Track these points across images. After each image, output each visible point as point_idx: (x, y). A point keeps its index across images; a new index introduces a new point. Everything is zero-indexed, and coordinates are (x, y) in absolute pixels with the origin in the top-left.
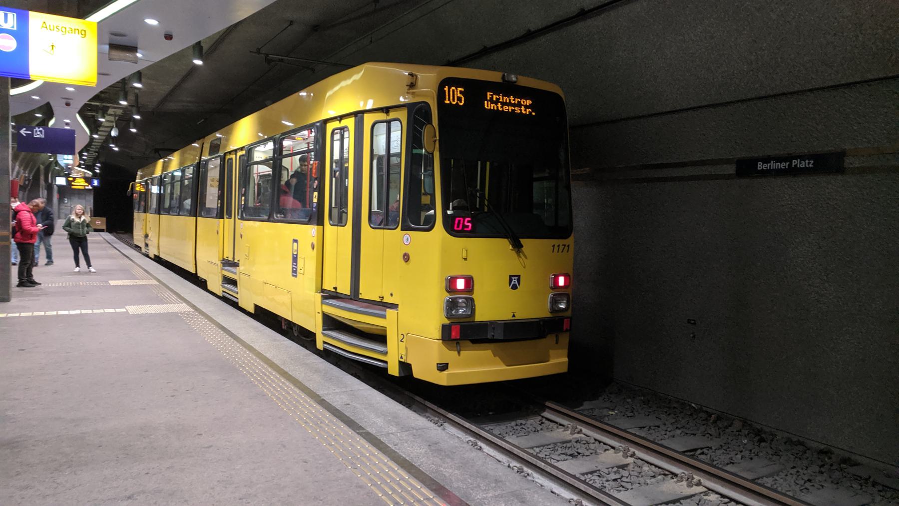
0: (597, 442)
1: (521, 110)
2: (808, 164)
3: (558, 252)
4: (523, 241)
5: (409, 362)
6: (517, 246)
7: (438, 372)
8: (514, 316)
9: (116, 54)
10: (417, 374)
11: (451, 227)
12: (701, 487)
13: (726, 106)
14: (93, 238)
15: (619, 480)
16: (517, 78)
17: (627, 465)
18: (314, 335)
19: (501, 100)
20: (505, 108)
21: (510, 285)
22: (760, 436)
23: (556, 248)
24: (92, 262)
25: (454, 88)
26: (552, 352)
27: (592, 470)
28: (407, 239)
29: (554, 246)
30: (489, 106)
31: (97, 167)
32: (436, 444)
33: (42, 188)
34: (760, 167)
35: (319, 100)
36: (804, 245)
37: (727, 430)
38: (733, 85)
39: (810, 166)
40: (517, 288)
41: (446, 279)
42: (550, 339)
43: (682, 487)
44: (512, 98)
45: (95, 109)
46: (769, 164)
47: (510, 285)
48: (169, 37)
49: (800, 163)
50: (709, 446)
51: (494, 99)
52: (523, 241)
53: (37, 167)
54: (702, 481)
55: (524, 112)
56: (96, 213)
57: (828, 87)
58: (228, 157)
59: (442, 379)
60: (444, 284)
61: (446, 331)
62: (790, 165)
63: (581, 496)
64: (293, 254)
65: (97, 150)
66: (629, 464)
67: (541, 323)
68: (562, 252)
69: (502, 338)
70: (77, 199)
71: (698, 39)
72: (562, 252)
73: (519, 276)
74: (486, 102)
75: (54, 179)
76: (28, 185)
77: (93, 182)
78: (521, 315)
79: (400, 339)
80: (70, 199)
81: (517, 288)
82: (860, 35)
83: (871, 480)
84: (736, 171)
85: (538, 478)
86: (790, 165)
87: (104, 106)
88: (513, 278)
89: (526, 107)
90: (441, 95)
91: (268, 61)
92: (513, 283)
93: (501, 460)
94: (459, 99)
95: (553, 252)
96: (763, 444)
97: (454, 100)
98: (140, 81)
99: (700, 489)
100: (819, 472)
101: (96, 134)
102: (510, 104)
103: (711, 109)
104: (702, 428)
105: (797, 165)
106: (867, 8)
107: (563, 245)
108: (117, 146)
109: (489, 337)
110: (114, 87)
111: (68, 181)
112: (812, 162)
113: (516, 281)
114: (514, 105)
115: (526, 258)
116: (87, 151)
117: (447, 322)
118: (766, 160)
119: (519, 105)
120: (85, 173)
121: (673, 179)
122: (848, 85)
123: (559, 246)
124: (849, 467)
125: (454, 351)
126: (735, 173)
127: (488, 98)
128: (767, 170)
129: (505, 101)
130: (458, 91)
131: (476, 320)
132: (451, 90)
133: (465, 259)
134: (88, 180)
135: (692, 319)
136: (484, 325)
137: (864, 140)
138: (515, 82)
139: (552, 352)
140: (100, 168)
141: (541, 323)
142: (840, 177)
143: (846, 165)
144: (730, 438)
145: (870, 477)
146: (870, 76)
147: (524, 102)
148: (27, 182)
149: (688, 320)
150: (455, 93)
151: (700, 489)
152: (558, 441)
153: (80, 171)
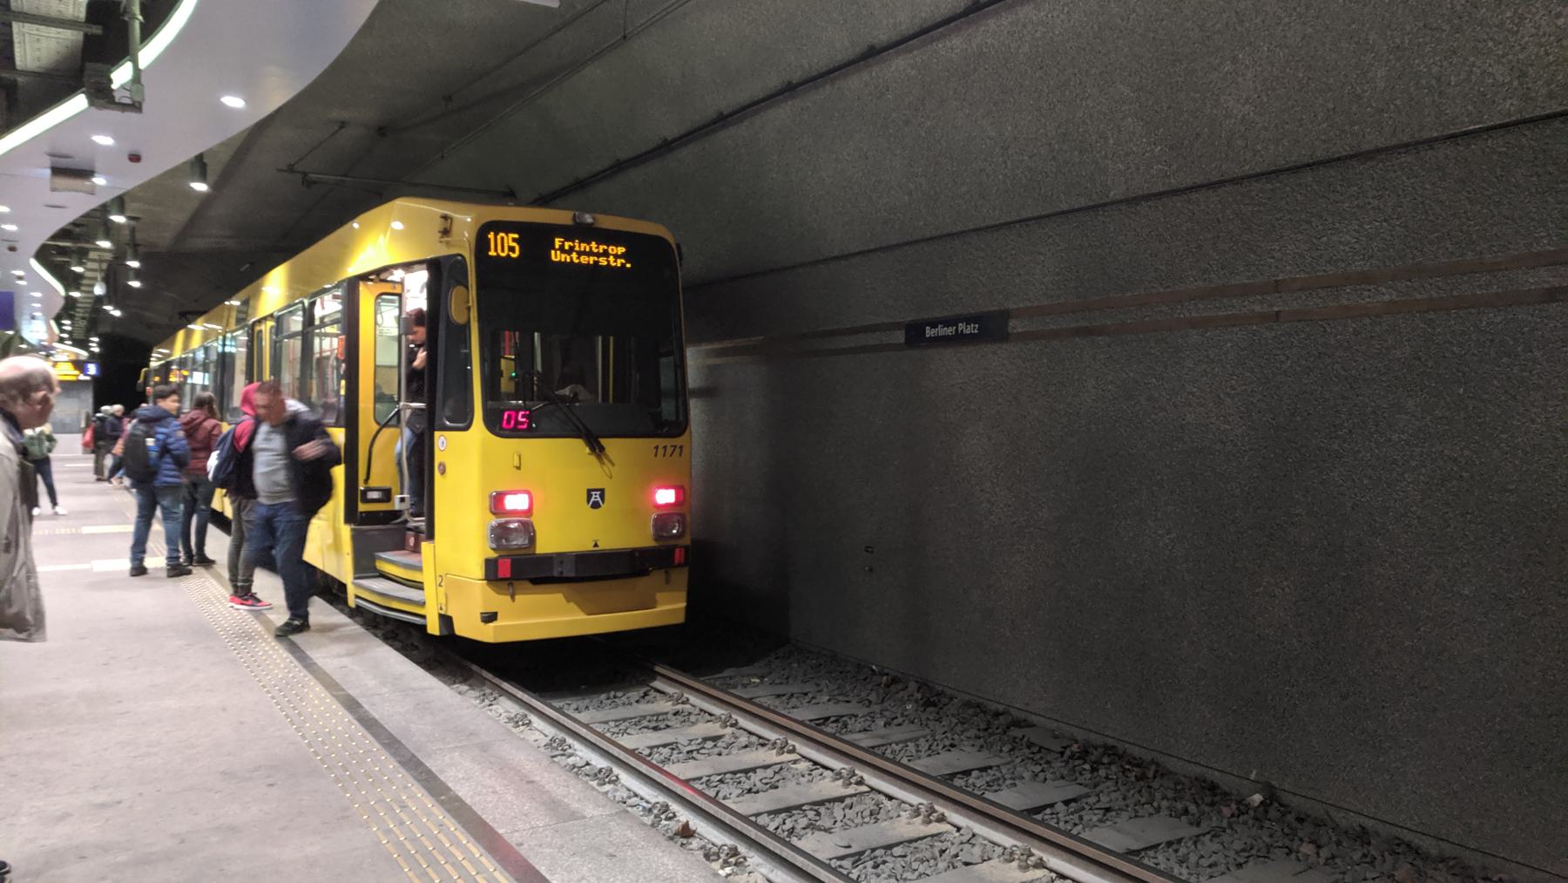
1: (609, 262)
3: (664, 455)
4: (603, 441)
5: (449, 614)
6: (597, 449)
7: (482, 624)
8: (596, 545)
10: (461, 629)
11: (495, 424)
16: (594, 219)
17: (720, 737)
18: (343, 587)
19: (577, 249)
20: (584, 260)
21: (588, 503)
22: (932, 700)
23: (661, 451)
24: (60, 499)
25: (503, 234)
26: (659, 596)
28: (443, 443)
29: (657, 448)
30: (558, 256)
31: (93, 342)
35: (344, 252)
41: (491, 496)
42: (657, 577)
44: (594, 245)
45: (63, 251)
47: (588, 502)
48: (135, 158)
50: (855, 714)
51: (567, 248)
52: (603, 441)
55: (613, 264)
57: (988, 227)
58: (257, 328)
59: (487, 634)
60: (487, 504)
61: (491, 566)
62: (957, 330)
63: (613, 762)
65: (87, 315)
67: (637, 554)
68: (671, 455)
69: (573, 575)
72: (671, 455)
73: (602, 491)
74: (553, 252)
77: (87, 370)
78: (603, 546)
79: (438, 583)
83: (1025, 739)
84: (906, 339)
85: (581, 751)
86: (957, 330)
87: (80, 248)
88: (593, 493)
89: (616, 256)
90: (481, 244)
91: (308, 183)
92: (593, 500)
94: (512, 249)
95: (656, 455)
96: (930, 709)
97: (503, 251)
98: (121, 212)
99: (794, 757)
100: (976, 737)
101: (77, 289)
102: (591, 253)
107: (672, 446)
108: (117, 307)
109: (556, 574)
110: (91, 217)
112: (977, 326)
113: (598, 496)
114: (598, 255)
115: (613, 464)
116: (71, 317)
117: (493, 555)
118: (934, 325)
119: (606, 254)
120: (77, 355)
122: (1008, 224)
123: (665, 447)
125: (506, 595)
127: (557, 247)
129: (582, 249)
130: (510, 239)
131: (537, 552)
132: (499, 237)
133: (518, 468)
134: (79, 365)
136: (548, 559)
138: (592, 224)
139: (659, 596)
140: (100, 345)
141: (637, 554)
142: (1005, 346)
143: (1010, 330)
146: (1025, 215)
147: (613, 250)
150: (505, 241)
151: (794, 757)
153: (64, 351)
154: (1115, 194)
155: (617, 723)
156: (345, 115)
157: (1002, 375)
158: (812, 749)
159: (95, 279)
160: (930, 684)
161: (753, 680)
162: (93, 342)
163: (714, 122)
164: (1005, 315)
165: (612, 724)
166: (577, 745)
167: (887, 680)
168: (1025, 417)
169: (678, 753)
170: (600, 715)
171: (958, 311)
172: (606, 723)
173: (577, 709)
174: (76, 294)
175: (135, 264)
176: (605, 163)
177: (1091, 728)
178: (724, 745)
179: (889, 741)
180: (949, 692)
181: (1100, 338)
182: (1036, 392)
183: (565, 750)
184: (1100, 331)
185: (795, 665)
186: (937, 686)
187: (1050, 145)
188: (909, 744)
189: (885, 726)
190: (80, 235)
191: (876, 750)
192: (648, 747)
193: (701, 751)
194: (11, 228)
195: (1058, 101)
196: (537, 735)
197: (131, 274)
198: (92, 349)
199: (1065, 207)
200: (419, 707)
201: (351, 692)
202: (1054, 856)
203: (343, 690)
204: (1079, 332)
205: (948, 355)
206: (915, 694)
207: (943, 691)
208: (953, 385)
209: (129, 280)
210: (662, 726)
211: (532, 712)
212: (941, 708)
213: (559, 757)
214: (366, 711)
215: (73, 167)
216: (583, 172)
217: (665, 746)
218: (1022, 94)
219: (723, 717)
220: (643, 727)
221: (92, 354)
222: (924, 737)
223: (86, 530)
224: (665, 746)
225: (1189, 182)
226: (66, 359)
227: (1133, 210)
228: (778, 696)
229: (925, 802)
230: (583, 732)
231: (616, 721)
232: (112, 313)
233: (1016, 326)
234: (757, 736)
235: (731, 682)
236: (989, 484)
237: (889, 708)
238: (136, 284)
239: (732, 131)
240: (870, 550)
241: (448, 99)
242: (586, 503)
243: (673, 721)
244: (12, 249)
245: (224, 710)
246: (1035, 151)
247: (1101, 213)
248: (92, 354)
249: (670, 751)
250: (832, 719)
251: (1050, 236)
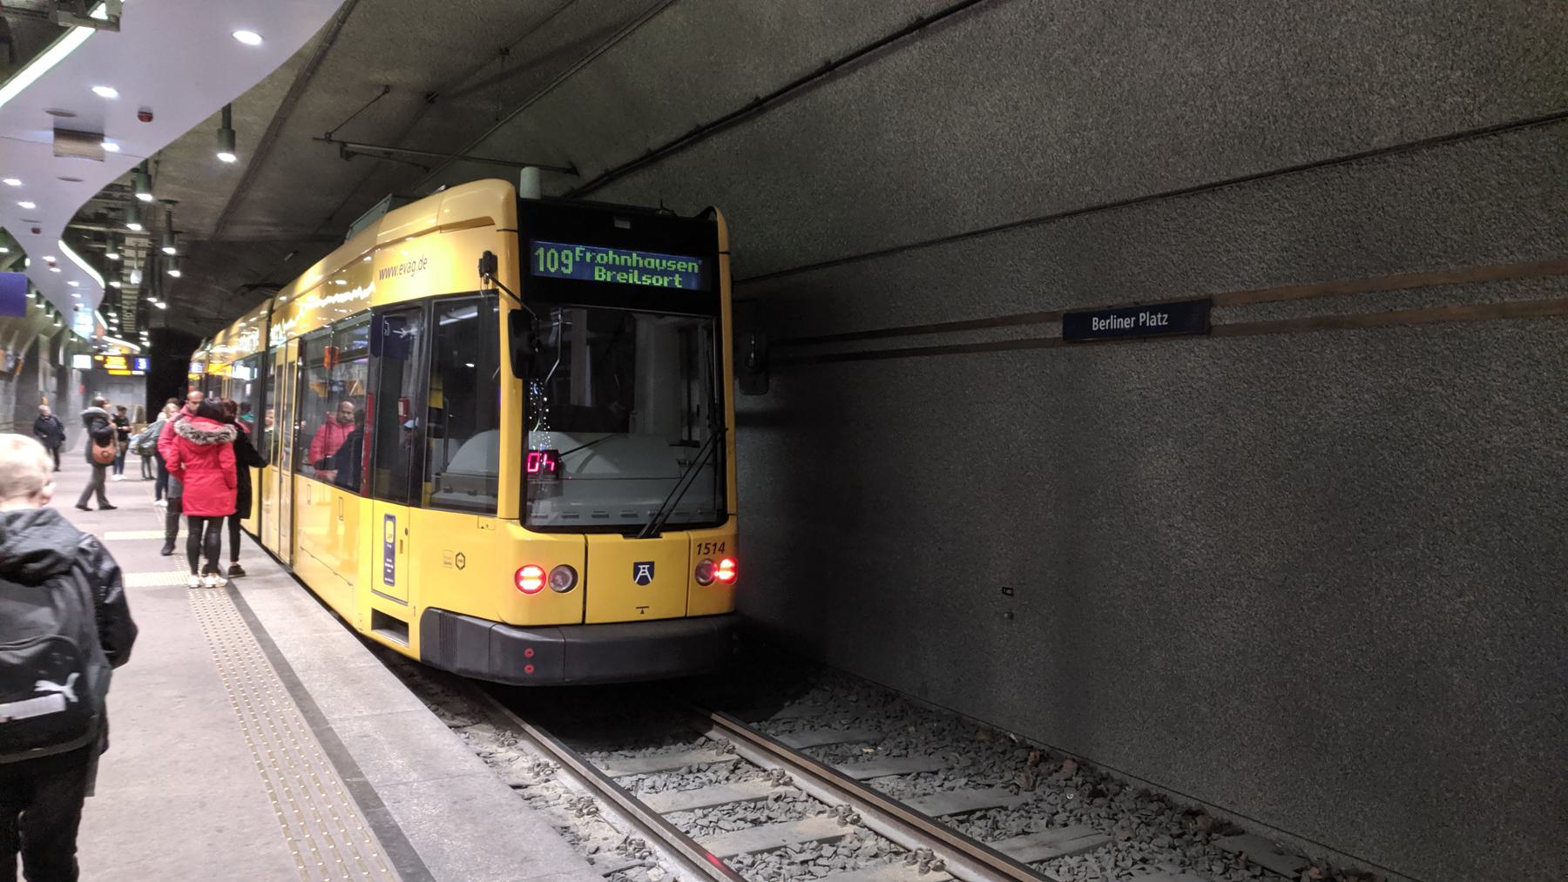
0: (811, 800)
9: (67, 146)
12: (945, 872)
13: (1048, 223)
15: (811, 863)
17: (840, 838)
21: (635, 578)
22: (1098, 788)
27: (773, 846)
32: (467, 800)
33: (45, 375)
34: (600, 276)
36: (1161, 457)
37: (1050, 778)
38: (1054, 188)
39: (1164, 323)
40: (648, 582)
43: (911, 873)
46: (1108, 321)
49: (1150, 319)
50: (1004, 805)
53: (32, 339)
54: (947, 861)
62: (1137, 321)
64: (386, 543)
66: (844, 836)
70: (118, 392)
71: (997, 111)
73: (652, 564)
75: (68, 360)
81: (648, 582)
82: (1217, 104)
83: (1243, 857)
84: (1064, 333)
86: (1137, 321)
91: (347, 155)
92: (640, 574)
93: (620, 830)
96: (1098, 801)
98: (149, 188)
103: (1027, 228)
104: (1008, 776)
105: (1146, 321)
106: (1222, 61)
108: (161, 299)
111: (94, 362)
112: (1166, 316)
118: (1104, 315)
120: (132, 350)
121: (977, 348)
122: (1211, 187)
124: (1222, 837)
126: (1061, 336)
132: (549, 255)
135: (1008, 586)
137: (1236, 279)
140: (150, 338)
142: (1206, 342)
143: (1213, 321)
144: (1048, 791)
145: (1241, 853)
146: (1240, 173)
149: (1003, 588)
152: (743, 798)
154: (1380, 141)
155: (706, 812)
156: (391, 77)
157: (1202, 379)
158: (967, 866)
159: (132, 268)
160: (1091, 765)
161: (865, 750)
162: (143, 336)
163: (819, 73)
164: (1207, 303)
165: (699, 813)
166: (659, 851)
167: (1035, 756)
168: (1235, 433)
169: (789, 864)
170: (684, 799)
171: (1138, 297)
172: (692, 810)
173: (653, 787)
174: (116, 284)
175: (170, 251)
176: (683, 129)
177: (1332, 845)
178: (846, 852)
179: (1059, 853)
180: (1117, 776)
181: (1352, 332)
182: (1252, 403)
183: (644, 858)
184: (1354, 324)
185: (912, 729)
186: (1099, 768)
187: (1283, 79)
188: (1087, 856)
189: (1047, 826)
190: (115, 219)
192: (749, 853)
193: (818, 862)
194: (28, 205)
195: (1301, 19)
196: (607, 831)
197: (171, 263)
198: (144, 343)
199: (1300, 160)
200: (457, 807)
201: (370, 778)
203: (360, 774)
204: (1318, 324)
205: (1123, 353)
206: (1073, 778)
207: (1108, 774)
208: (1129, 391)
209: (168, 269)
210: (763, 819)
211: (600, 796)
212: (1112, 800)
213: (637, 869)
214: (387, 813)
215: (76, 128)
216: (657, 141)
217: (770, 851)
218: (1248, 12)
219: (841, 809)
220: (739, 819)
222: (1104, 845)
224: (770, 851)
225: (1506, 118)
226: (119, 353)
227: (1409, 161)
228: (902, 776)
230: (668, 836)
231: (704, 808)
232: (157, 305)
233: (1221, 317)
234: (887, 839)
235: (838, 751)
236: (1180, 518)
237: (1045, 797)
238: (175, 274)
239: (841, 83)
240: (1009, 592)
241: (505, 52)
242: (50, 107)
243: (777, 810)
244: (36, 231)
245: (203, 805)
246: (1260, 88)
247: (1355, 167)
249: (777, 859)
250: (978, 814)
251: (1276, 200)
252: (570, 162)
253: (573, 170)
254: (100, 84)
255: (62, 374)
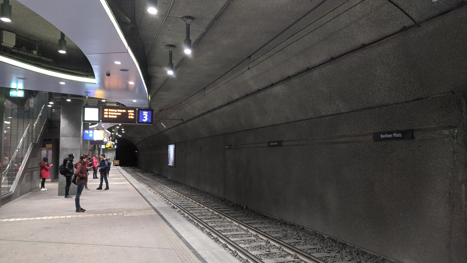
2: (399, 135)
14: (112, 167)
46: (385, 135)
49: (397, 135)
56: (117, 158)
70: (110, 153)
76: (92, 149)
80: (107, 153)
86: (393, 135)
108: (120, 135)
112: (401, 134)
118: (384, 134)
120: (113, 143)
128: (391, 137)
140: (117, 141)
148: (92, 149)
164: (282, 141)
191: (277, 238)
202: (261, 236)
221: (115, 143)
223: (113, 179)
229: (294, 254)
248: (115, 143)
252: (182, 118)
253: (183, 120)
254: (60, 50)
255: (99, 149)
